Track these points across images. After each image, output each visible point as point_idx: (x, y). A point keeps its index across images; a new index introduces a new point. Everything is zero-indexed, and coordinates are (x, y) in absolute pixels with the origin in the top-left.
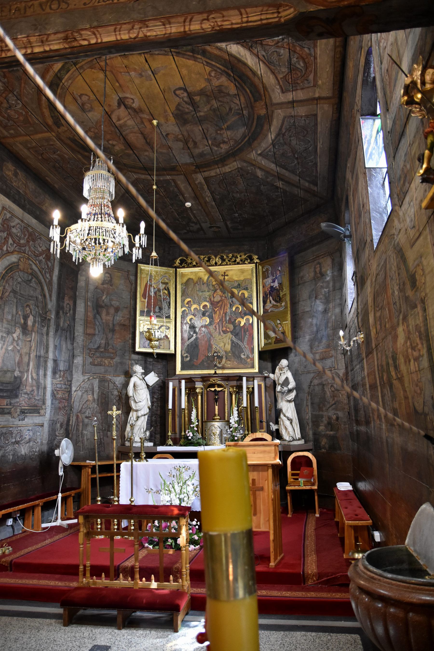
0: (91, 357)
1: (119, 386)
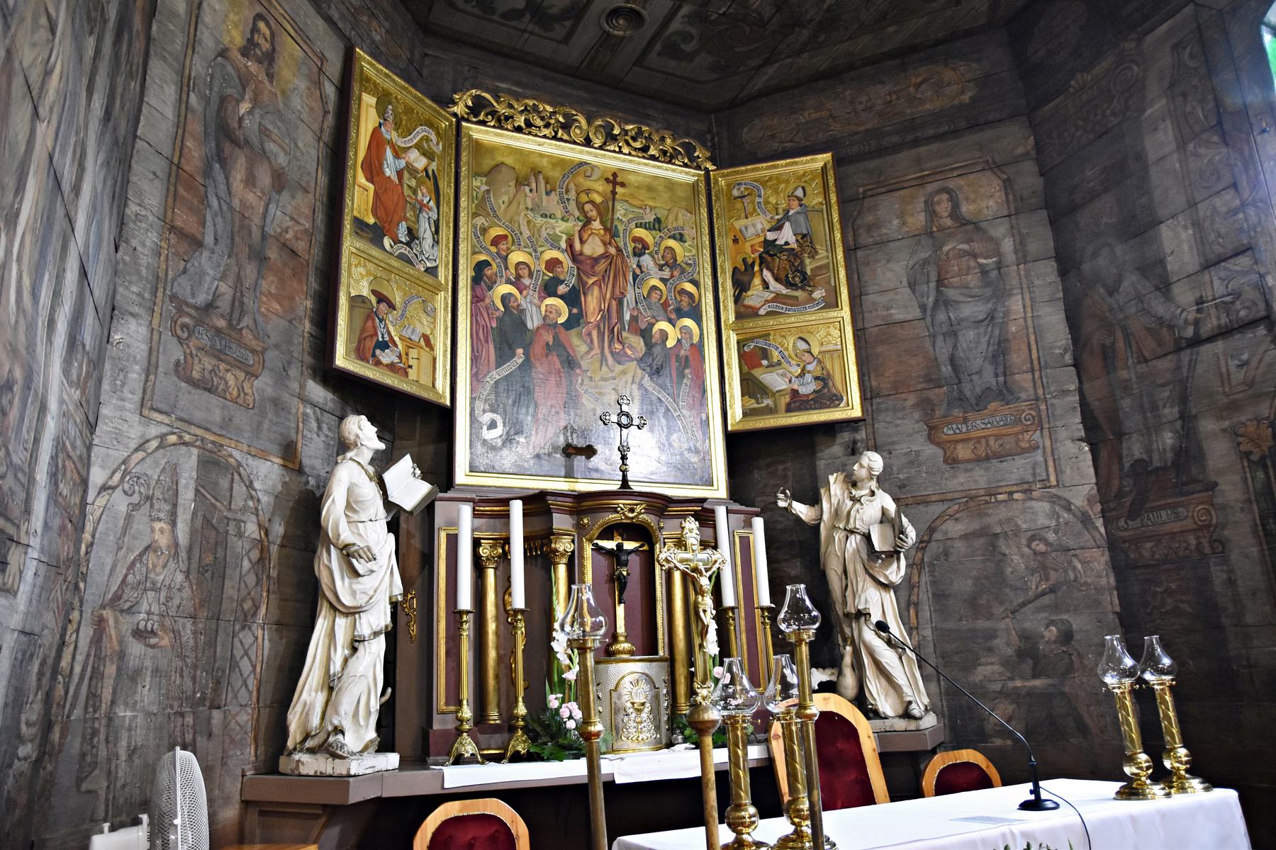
1: (264, 499)
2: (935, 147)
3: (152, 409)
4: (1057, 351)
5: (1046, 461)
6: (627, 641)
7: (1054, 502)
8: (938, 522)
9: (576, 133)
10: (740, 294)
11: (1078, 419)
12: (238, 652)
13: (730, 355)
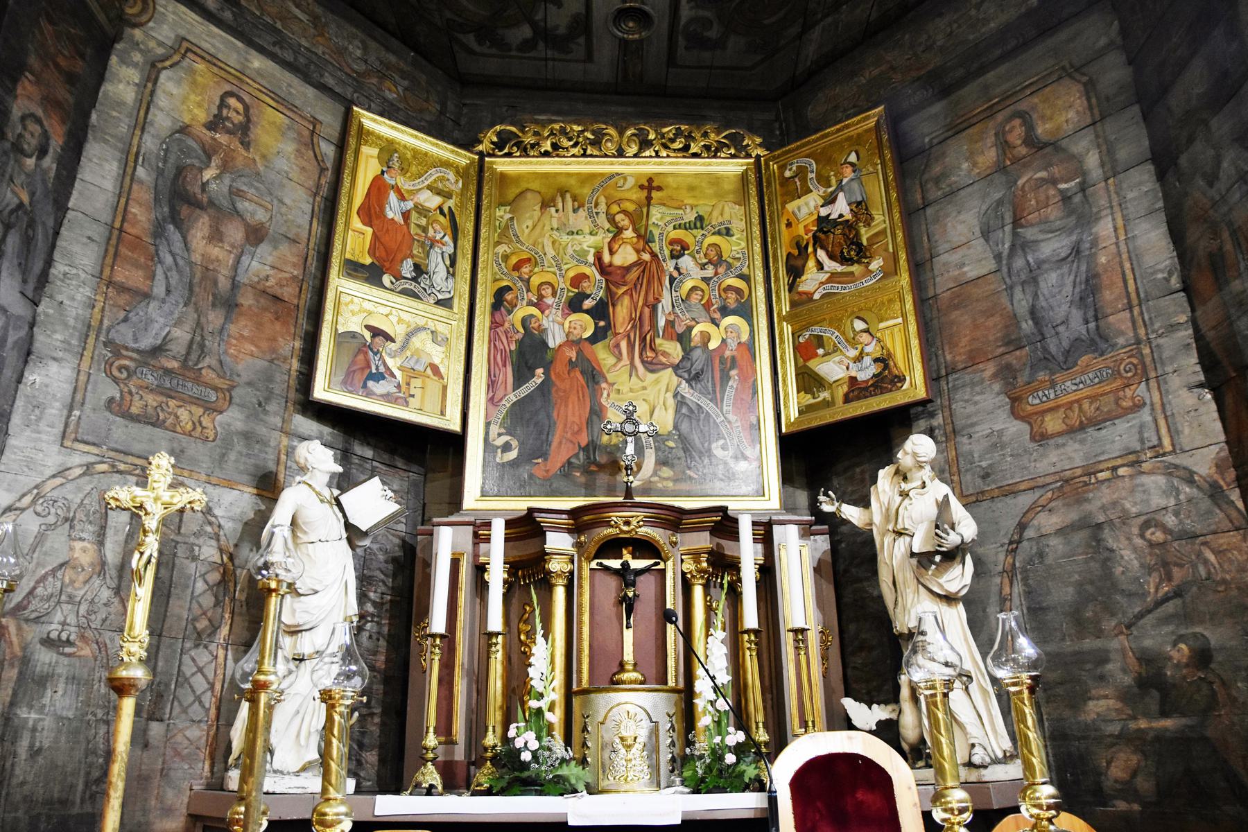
0: (116, 380)
1: (228, 525)
2: (1002, 69)
3: (76, 440)
4: (1160, 276)
5: (1155, 421)
6: (635, 670)
7: (1170, 474)
8: (1030, 516)
9: (610, 147)
10: (794, 281)
11: (1194, 359)
12: (188, 669)
13: (783, 352)
